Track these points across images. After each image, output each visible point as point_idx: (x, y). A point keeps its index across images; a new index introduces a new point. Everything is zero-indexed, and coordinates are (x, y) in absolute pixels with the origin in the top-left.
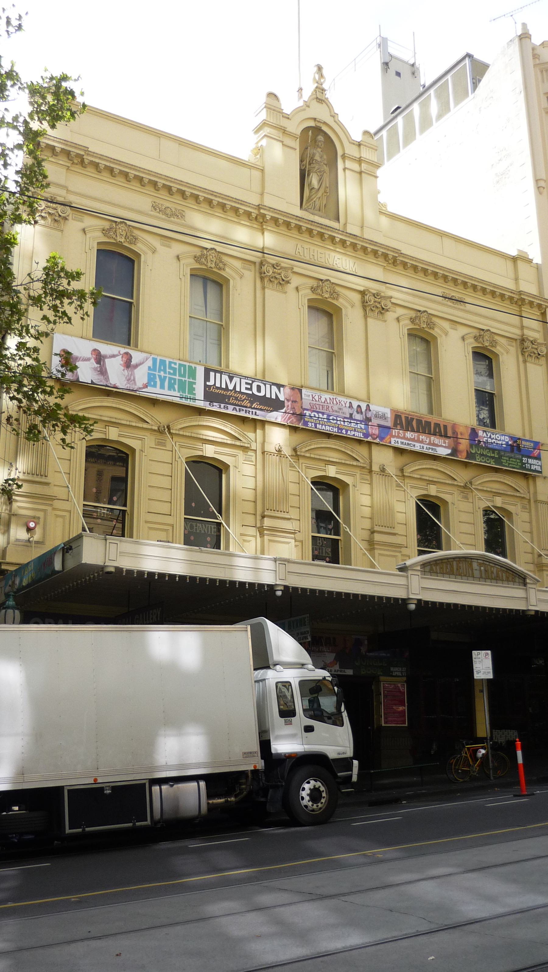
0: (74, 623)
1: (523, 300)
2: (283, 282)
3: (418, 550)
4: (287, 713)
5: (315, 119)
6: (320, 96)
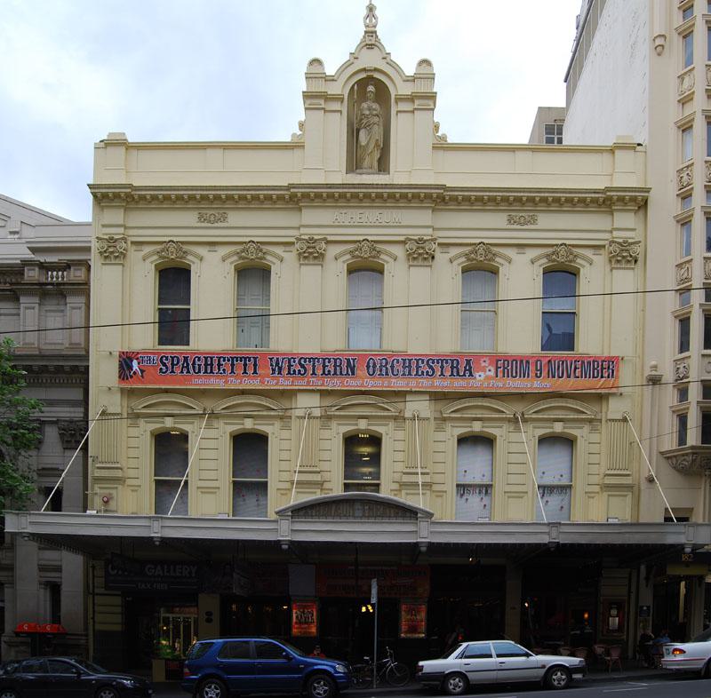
0: (614, 546)
1: (610, 198)
2: (320, 257)
3: (345, 484)
4: (209, 621)
5: (364, 70)
6: (371, 41)
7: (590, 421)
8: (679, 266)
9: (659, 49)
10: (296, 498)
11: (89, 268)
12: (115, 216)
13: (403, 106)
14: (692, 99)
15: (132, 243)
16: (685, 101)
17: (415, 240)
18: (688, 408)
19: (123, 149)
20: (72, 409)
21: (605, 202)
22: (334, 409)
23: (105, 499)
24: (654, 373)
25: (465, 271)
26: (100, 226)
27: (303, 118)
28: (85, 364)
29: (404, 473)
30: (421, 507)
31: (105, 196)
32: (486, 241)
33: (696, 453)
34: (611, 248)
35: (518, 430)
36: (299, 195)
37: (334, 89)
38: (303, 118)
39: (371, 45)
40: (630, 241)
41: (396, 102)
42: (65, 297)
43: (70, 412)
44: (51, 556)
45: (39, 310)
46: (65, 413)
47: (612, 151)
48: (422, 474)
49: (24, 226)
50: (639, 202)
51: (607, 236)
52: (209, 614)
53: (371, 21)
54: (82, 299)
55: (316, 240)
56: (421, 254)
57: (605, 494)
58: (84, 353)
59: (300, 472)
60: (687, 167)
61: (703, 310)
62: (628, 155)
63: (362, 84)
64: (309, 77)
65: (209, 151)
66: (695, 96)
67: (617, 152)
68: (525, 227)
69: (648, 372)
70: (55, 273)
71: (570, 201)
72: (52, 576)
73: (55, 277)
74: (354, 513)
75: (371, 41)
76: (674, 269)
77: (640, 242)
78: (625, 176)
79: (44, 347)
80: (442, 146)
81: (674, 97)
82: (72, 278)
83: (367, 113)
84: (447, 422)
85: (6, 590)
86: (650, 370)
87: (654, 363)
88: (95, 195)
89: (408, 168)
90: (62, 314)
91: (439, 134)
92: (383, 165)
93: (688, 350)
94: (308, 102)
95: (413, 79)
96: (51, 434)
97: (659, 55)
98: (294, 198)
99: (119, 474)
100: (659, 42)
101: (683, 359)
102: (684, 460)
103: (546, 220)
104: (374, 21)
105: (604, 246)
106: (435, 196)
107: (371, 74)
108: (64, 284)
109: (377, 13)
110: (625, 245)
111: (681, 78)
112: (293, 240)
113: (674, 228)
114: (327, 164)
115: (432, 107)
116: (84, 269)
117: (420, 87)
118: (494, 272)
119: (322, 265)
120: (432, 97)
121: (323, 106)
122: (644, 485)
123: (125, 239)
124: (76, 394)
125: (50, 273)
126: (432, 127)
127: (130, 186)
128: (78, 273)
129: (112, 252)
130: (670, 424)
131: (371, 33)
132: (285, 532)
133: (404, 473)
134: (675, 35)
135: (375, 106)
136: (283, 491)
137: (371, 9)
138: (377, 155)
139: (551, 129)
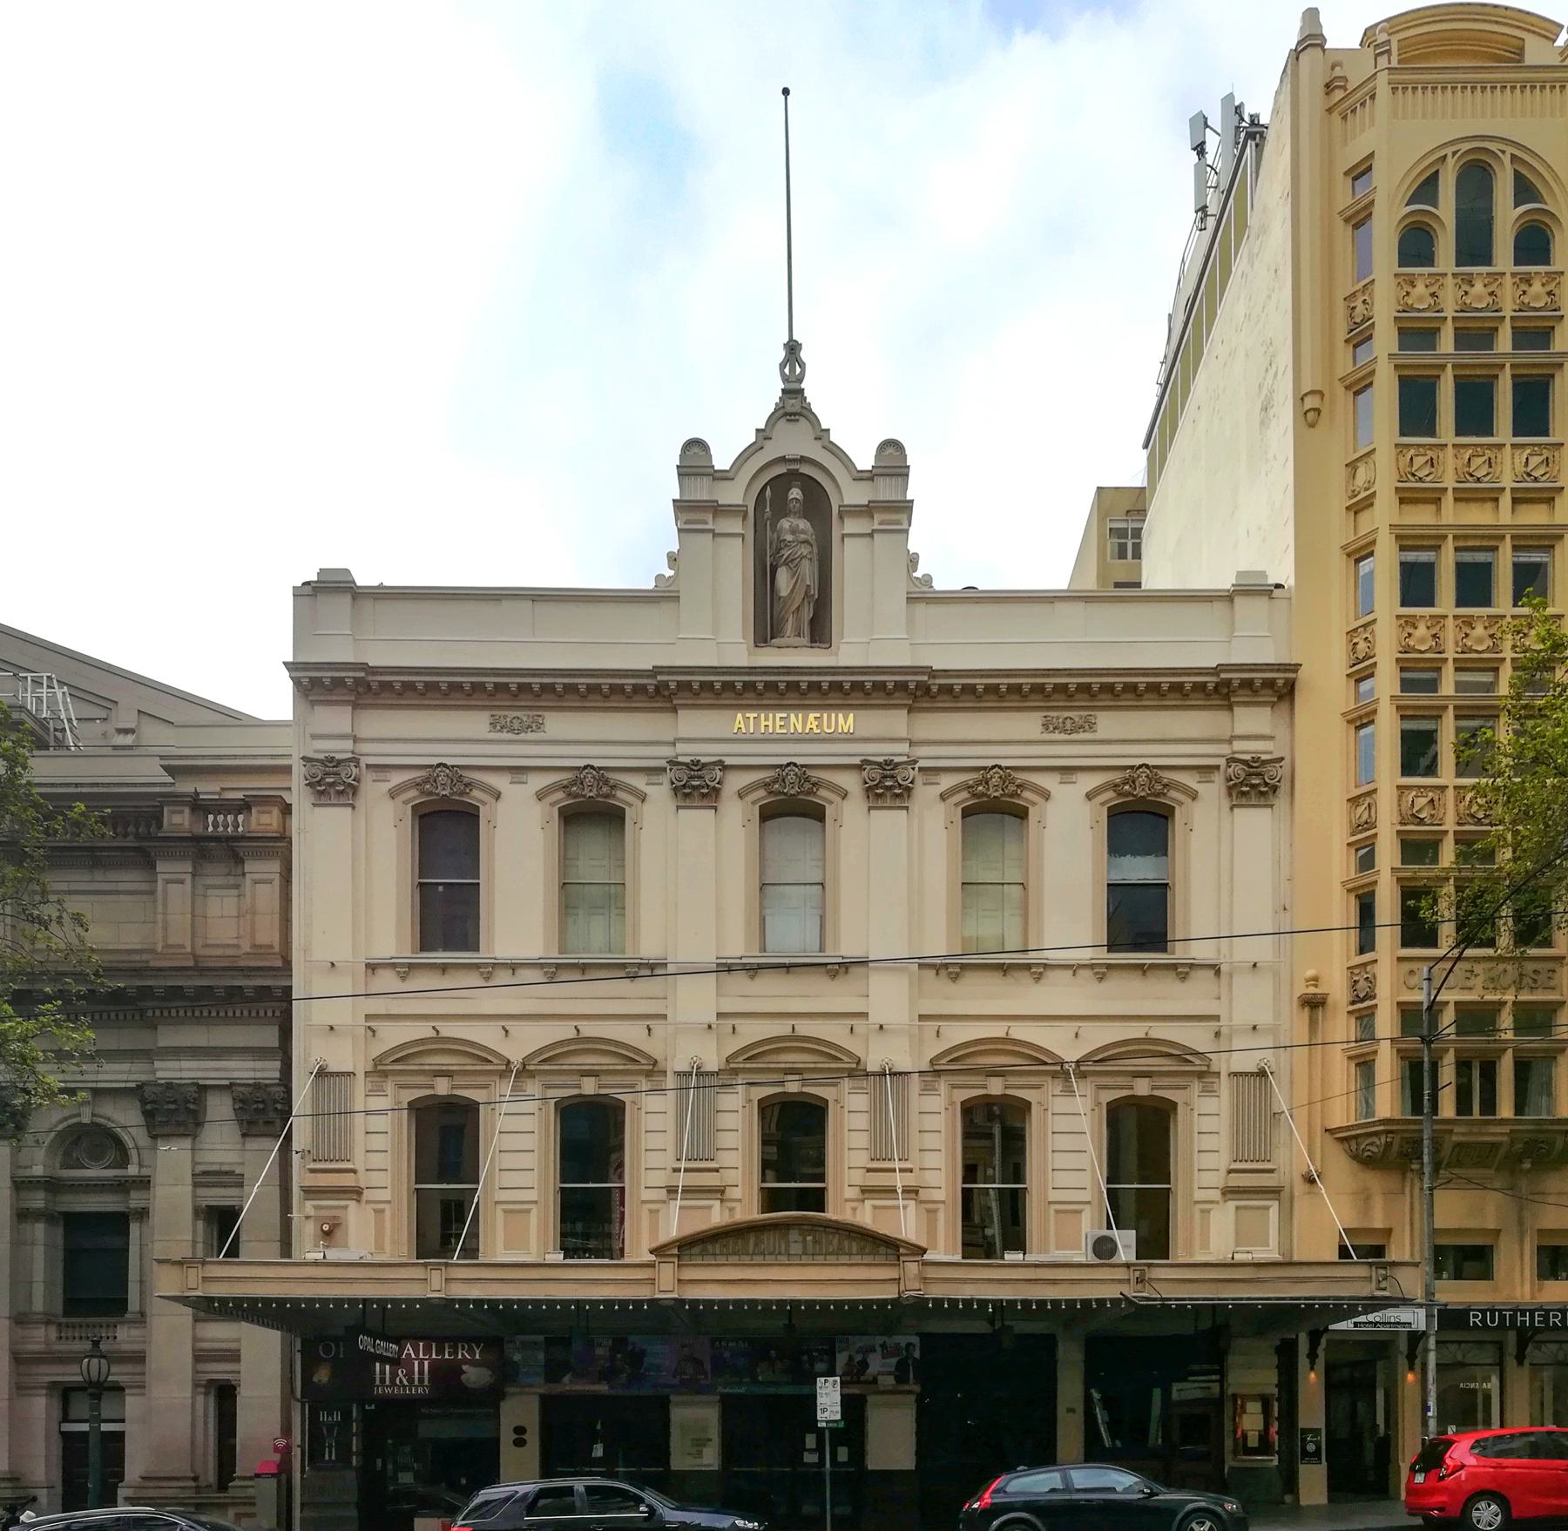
1: (1228, 682)
6: (793, 406)
7: (1201, 1075)
8: (1354, 801)
9: (1311, 415)
10: (673, 1225)
11: (287, 810)
12: (336, 719)
13: (851, 526)
14: (1372, 505)
15: (368, 766)
16: (1360, 506)
17: (879, 764)
18: (1375, 1052)
19: (348, 598)
20: (259, 1064)
21: (1221, 689)
22: (741, 1059)
23: (326, 1228)
24: (1312, 990)
25: (967, 813)
26: (308, 739)
27: (675, 548)
28: (285, 983)
29: (869, 1170)
30: (903, 1236)
31: (315, 682)
32: (1004, 763)
33: (1391, 1132)
34: (1230, 770)
35: (1069, 1092)
36: (673, 686)
37: (733, 494)
38: (675, 548)
39: (795, 414)
40: (1264, 757)
41: (841, 517)
42: (239, 861)
43: (254, 1070)
44: (220, 1332)
45: (194, 886)
46: (244, 1070)
47: (1228, 597)
48: (902, 1170)
49: (145, 719)
50: (1277, 687)
51: (1225, 749)
52: (520, 1430)
53: (792, 370)
54: (274, 867)
55: (705, 765)
56: (888, 786)
57: (1232, 1205)
58: (279, 963)
59: (686, 1170)
60: (1365, 626)
61: (1399, 879)
62: (1261, 603)
63: (780, 484)
64: (684, 472)
65: (505, 604)
66: (1377, 501)
67: (1238, 600)
68: (1074, 736)
69: (1302, 989)
70: (221, 818)
71: (1154, 688)
72: (219, 1371)
73: (214, 824)
74: (787, 1249)
75: (793, 406)
76: (1345, 805)
77: (1282, 759)
78: (1251, 643)
79: (201, 952)
80: (922, 596)
81: (1338, 502)
82: (253, 826)
83: (789, 538)
84: (943, 1079)
85: (128, 1399)
86: (1304, 984)
87: (1311, 973)
88: (297, 682)
89: (866, 638)
90: (234, 892)
91: (918, 574)
92: (819, 631)
93: (1373, 949)
94: (686, 516)
95: (868, 477)
96: (220, 1108)
97: (1312, 425)
98: (663, 691)
99: (347, 1180)
100: (1310, 402)
101: (1365, 965)
102: (1371, 1144)
103: (1110, 723)
104: (798, 370)
105: (1217, 767)
106: (912, 686)
107: (796, 467)
108: (243, 838)
109: (803, 355)
110: (1255, 766)
111: (1352, 466)
112: (663, 763)
113: (1339, 732)
114: (720, 638)
115: (904, 526)
116: (276, 812)
117: (884, 491)
118: (1021, 814)
119: (716, 809)
120: (906, 507)
121: (710, 526)
122: (1300, 1187)
123: (355, 760)
124: (268, 1036)
125: (211, 818)
126: (904, 562)
127: (364, 667)
128: (265, 819)
129: (332, 785)
130: (1341, 1073)
131: (793, 392)
132: (667, 1284)
133: (869, 1170)
134: (1340, 390)
135: (803, 524)
136: (654, 1212)
137: (793, 348)
138: (807, 614)
139: (1120, 523)
